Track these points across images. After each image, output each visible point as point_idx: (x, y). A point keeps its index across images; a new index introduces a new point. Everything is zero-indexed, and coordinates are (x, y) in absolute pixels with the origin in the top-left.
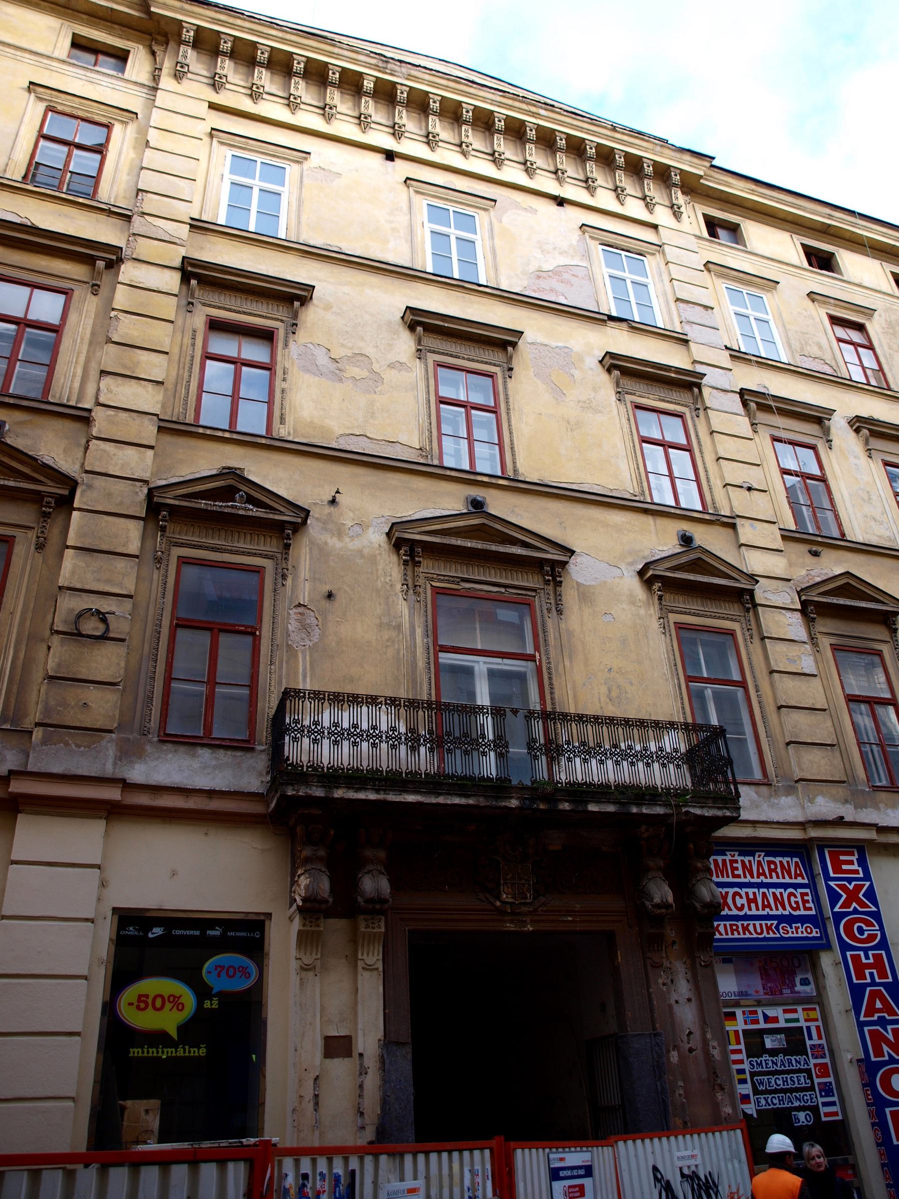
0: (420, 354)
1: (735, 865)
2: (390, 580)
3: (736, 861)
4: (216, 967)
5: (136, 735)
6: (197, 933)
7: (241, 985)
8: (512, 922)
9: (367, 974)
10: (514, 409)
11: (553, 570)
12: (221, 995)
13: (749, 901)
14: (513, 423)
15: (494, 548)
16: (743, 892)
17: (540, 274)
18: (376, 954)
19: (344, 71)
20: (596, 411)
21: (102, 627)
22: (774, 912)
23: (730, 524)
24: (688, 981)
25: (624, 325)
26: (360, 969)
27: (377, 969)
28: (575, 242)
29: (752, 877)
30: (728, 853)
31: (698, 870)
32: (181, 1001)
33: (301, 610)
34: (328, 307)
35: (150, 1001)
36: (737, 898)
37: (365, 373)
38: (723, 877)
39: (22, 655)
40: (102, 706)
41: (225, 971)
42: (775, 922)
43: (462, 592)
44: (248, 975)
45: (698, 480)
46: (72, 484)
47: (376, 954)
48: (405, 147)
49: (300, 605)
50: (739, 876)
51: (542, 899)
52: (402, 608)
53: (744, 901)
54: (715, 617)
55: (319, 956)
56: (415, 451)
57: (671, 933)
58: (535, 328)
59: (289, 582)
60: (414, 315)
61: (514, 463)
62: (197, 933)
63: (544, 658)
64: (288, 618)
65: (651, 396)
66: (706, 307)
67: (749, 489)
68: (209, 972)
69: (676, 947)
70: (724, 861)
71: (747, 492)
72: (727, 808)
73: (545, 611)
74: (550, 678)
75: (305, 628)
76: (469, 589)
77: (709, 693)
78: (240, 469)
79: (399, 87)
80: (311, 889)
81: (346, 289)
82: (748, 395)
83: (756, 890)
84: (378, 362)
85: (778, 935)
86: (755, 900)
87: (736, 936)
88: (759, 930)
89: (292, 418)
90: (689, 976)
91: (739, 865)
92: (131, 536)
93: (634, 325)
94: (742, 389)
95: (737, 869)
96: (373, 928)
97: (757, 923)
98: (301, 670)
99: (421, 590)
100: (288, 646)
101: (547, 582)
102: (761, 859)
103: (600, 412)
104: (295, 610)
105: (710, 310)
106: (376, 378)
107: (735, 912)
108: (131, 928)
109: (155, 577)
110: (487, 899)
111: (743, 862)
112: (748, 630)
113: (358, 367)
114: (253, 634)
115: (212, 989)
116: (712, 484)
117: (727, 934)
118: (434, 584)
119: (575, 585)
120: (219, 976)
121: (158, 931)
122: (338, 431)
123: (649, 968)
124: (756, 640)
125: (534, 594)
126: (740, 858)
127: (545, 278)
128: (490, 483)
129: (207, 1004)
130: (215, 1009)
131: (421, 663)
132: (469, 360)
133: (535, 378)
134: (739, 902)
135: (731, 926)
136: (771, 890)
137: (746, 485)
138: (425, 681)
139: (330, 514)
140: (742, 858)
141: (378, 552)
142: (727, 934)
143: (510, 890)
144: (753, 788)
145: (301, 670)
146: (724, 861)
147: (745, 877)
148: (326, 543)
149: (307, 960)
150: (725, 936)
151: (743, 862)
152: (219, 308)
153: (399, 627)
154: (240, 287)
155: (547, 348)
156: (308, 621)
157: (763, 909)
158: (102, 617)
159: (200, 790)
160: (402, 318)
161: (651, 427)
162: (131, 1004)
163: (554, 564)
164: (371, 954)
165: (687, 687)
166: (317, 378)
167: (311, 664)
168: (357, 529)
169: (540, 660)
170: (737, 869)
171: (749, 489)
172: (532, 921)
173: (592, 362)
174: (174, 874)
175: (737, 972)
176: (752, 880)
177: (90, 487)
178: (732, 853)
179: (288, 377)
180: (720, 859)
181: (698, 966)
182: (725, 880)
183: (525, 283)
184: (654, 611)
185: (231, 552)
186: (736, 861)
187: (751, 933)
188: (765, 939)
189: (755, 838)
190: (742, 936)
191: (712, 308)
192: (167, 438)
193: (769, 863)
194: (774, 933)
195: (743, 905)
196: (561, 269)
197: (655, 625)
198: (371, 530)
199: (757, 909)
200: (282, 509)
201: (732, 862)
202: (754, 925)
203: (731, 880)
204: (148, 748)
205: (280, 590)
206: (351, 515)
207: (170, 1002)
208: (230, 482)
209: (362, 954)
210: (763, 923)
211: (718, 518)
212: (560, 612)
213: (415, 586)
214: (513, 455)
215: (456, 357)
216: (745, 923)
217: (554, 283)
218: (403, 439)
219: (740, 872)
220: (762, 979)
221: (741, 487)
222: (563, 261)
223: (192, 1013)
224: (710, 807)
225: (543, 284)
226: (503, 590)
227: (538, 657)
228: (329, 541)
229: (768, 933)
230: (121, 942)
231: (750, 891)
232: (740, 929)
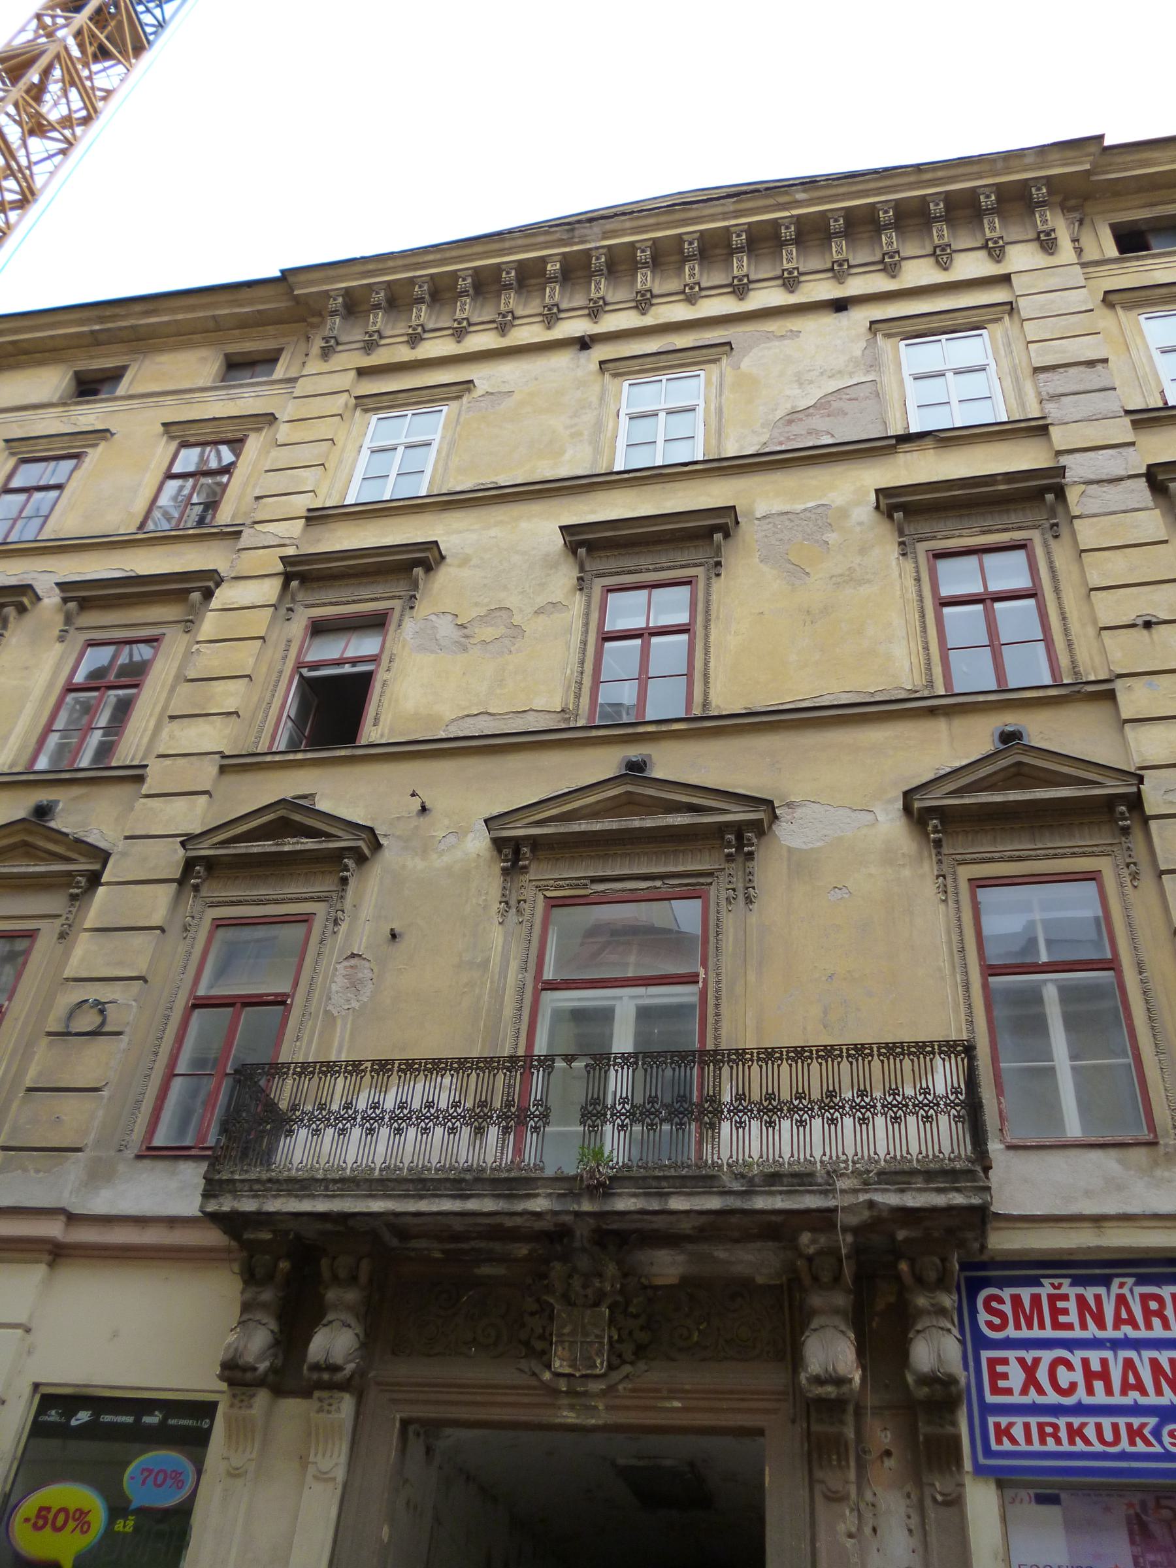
0: (905, 550)
1: (1060, 1304)
2: (485, 900)
3: (1065, 1297)
4: (143, 1470)
5: (112, 1153)
6: (130, 1419)
7: (169, 1499)
8: (572, 1407)
9: (318, 1487)
10: (718, 618)
11: (740, 837)
12: (142, 1511)
13: (1089, 1376)
14: (712, 638)
15: (637, 823)
16: (1076, 1358)
17: (793, 417)
18: (336, 1454)
19: (898, 205)
20: (862, 582)
21: (98, 1020)
22: (1152, 1399)
23: (1104, 694)
24: (910, 1531)
25: (928, 442)
26: (309, 1478)
27: (334, 1479)
28: (858, 353)
29: (1101, 1325)
30: (1045, 1281)
31: (921, 1312)
32: (88, 1518)
33: (353, 962)
34: (465, 561)
35: (51, 1516)
36: (1061, 1370)
37: (502, 630)
38: (1030, 1327)
39: (14, 1068)
40: (75, 1118)
41: (153, 1476)
42: (1152, 1421)
43: (592, 899)
44: (180, 1484)
45: (1048, 640)
46: (104, 856)
47: (336, 1454)
48: (856, 286)
49: (353, 956)
50: (1070, 1326)
51: (627, 1369)
52: (496, 936)
53: (1078, 1376)
54: (1055, 857)
55: (254, 1455)
56: (554, 716)
57: (882, 1436)
58: (451, 533)
59: (343, 928)
60: (572, 535)
61: (706, 693)
62: (130, 1419)
63: (712, 975)
64: (334, 975)
65: (964, 532)
66: (1091, 363)
67: (1148, 625)
68: (132, 1478)
69: (889, 1463)
70: (1036, 1299)
71: (1145, 632)
72: (958, 1190)
73: (723, 903)
74: (717, 1006)
75: (354, 984)
76: (603, 892)
77: (1051, 994)
78: (304, 797)
79: (594, 253)
80: (232, 1350)
81: (493, 532)
82: (1165, 472)
83: (1108, 1354)
84: (521, 610)
85: (1158, 1449)
86: (1104, 1375)
87: (1051, 1445)
88: (1109, 1436)
89: (390, 716)
90: (915, 1521)
91: (1072, 1305)
92: (157, 904)
93: (943, 435)
94: (1149, 466)
95: (1065, 1312)
96: (329, 1412)
97: (1106, 1422)
98: (336, 1044)
99: (526, 906)
100: (326, 1012)
101: (730, 858)
102: (1125, 1291)
103: (869, 581)
104: (346, 963)
105: (1100, 367)
106: (516, 631)
107: (1052, 1398)
108: (53, 1412)
109: (180, 949)
110: (530, 1369)
111: (1081, 1300)
112: (1128, 865)
113: (492, 626)
114: (283, 1003)
115: (130, 1502)
116: (1073, 637)
117: (1029, 1441)
118: (549, 894)
119: (785, 853)
120: (144, 1482)
121: (83, 1416)
122: (449, 715)
123: (819, 1499)
124: (1147, 880)
125: (709, 880)
126: (1072, 1292)
127: (801, 420)
128: (665, 731)
129: (119, 1526)
130: (127, 1533)
131: (508, 1011)
132: (656, 570)
133: (761, 565)
134: (1064, 1377)
135: (1041, 1426)
136: (1147, 1354)
137: (1140, 621)
138: (510, 1034)
139: (417, 827)
140: (1080, 1290)
141: (473, 865)
142: (1029, 1441)
143: (566, 1354)
144: (1113, 1153)
145: (336, 1044)
146: (1036, 1299)
147: (1084, 1326)
148: (404, 867)
149: (236, 1461)
150: (1023, 1447)
151: (1081, 1300)
152: (324, 605)
153: (485, 964)
154: (351, 572)
155: (790, 516)
156: (360, 975)
157: (1124, 1393)
158: (100, 1007)
159: (8, 1208)
160: (877, 508)
161: (960, 578)
162: (27, 1520)
163: (739, 829)
164: (328, 1454)
165: (985, 986)
166: (433, 656)
167: (352, 1034)
168: (452, 839)
169: (705, 980)
170: (1065, 1312)
171: (1148, 625)
172: (608, 1408)
173: (864, 512)
174: (115, 1335)
175: (1071, 1526)
176: (1101, 1334)
177: (124, 854)
178: (1056, 1282)
179: (395, 665)
180: (1026, 1294)
181: (928, 1502)
182: (1036, 1333)
183: (765, 438)
184: (928, 868)
185: (277, 902)
186: (1065, 1297)
187: (1087, 1442)
188: (1123, 1456)
189: (1099, 1248)
190: (1066, 1447)
191: (1106, 361)
192: (231, 779)
193: (1145, 1299)
194: (1148, 1443)
195: (1073, 1386)
196: (830, 398)
197: (929, 889)
198: (470, 836)
199: (1109, 1391)
200: (340, 833)
201: (1052, 1299)
202: (1099, 1427)
203: (1049, 1333)
204: (121, 1168)
205: (328, 942)
206: (446, 822)
207: (75, 1520)
208: (280, 813)
209: (316, 1455)
210: (1122, 1421)
211: (1076, 688)
212: (749, 900)
213: (519, 902)
214: (706, 683)
215: (636, 572)
216: (1077, 1421)
217: (817, 422)
218: (540, 703)
219: (1073, 1317)
220: (1132, 1542)
221: (1134, 626)
222: (833, 385)
223: (96, 1540)
224: (920, 1190)
225: (795, 429)
226: (658, 883)
227: (702, 976)
228: (410, 864)
229: (1132, 1443)
230: (38, 1430)
231: (1094, 1357)
232: (1063, 1434)
